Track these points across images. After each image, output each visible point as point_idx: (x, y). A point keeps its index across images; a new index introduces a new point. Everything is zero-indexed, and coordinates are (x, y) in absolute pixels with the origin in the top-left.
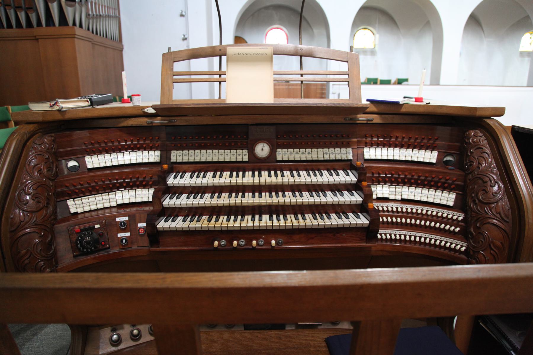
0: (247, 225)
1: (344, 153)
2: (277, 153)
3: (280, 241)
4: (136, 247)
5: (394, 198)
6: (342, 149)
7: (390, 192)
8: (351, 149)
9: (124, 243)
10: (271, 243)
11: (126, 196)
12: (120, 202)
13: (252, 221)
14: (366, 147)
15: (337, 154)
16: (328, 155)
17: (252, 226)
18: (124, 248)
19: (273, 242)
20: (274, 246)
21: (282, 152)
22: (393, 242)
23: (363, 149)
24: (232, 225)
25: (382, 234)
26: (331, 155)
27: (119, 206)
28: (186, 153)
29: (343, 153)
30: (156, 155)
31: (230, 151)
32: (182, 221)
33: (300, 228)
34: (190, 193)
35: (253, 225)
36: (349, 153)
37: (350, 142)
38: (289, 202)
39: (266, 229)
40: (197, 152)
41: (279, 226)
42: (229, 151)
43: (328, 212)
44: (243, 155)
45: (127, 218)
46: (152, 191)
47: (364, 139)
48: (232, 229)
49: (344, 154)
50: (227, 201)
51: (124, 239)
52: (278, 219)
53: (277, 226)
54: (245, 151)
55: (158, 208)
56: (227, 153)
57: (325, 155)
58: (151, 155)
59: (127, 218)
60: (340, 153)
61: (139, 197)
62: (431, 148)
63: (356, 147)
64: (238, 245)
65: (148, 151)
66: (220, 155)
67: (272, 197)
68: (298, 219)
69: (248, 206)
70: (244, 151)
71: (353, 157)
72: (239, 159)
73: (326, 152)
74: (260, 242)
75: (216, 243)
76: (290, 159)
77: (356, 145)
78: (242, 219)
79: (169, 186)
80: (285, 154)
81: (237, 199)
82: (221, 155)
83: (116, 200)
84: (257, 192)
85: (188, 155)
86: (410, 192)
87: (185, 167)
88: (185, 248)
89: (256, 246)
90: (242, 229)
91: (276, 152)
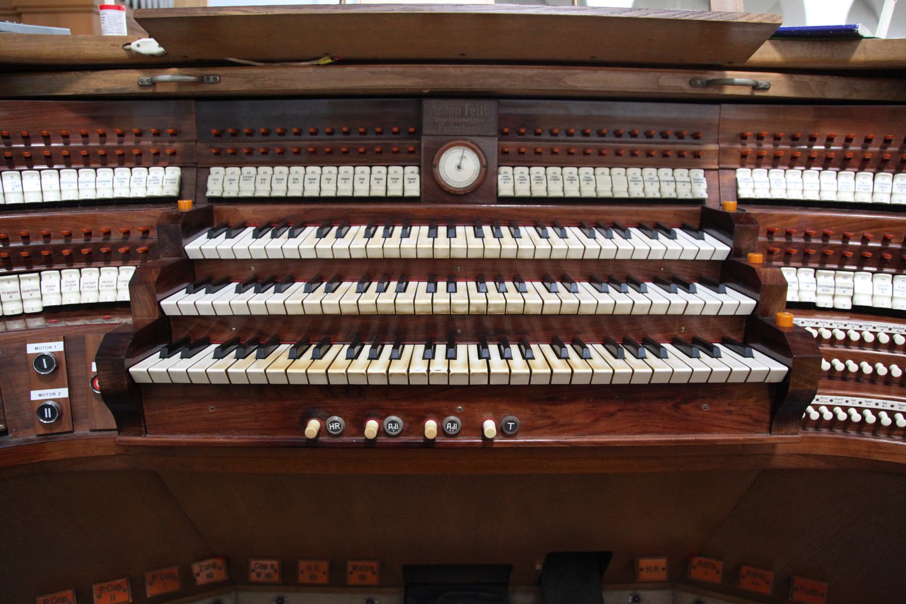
0: (408, 371)
1: (684, 182)
2: (500, 177)
3: (511, 424)
4: (88, 432)
5: (830, 306)
6: (678, 172)
7: (820, 286)
8: (703, 171)
9: (48, 419)
10: (482, 429)
11: (71, 284)
12: (53, 300)
13: (424, 358)
14: (743, 166)
15: (666, 183)
16: (576, 183)
17: (423, 374)
18: (48, 432)
19: (490, 427)
20: (492, 439)
21: (513, 175)
22: (882, 436)
23: (735, 173)
24: (363, 368)
25: (848, 407)
26: (648, 184)
27: (50, 312)
28: (249, 173)
29: (682, 182)
30: (167, 180)
31: (626, 172)
32: (212, 357)
33: (532, 383)
34: (386, 278)
35: (428, 370)
36: (698, 181)
37: (699, 151)
38: (536, 305)
39: (467, 383)
40: (297, 172)
41: (510, 374)
42: (366, 169)
43: (581, 337)
44: (406, 181)
45: (58, 346)
46: (128, 272)
47: (739, 146)
48: (363, 382)
49: (684, 185)
50: (352, 299)
51: (48, 406)
52: (506, 356)
53: (505, 374)
54: (412, 171)
55: (145, 315)
56: (362, 176)
57: (632, 185)
58: (156, 179)
59: (58, 346)
60: (672, 181)
61: (109, 288)
62: (158, 159)
63: (717, 167)
64: (381, 432)
65: (131, 168)
66: (342, 179)
67: (487, 292)
68: (566, 356)
69: (415, 316)
70: (408, 169)
71: (708, 192)
72: (395, 190)
73: (633, 178)
74: (449, 426)
75: (313, 426)
76: (535, 194)
77: (716, 161)
78: (396, 355)
79: (191, 257)
80: (522, 179)
81: (382, 294)
82: (345, 179)
83: (852, 294)
84: (442, 280)
85: (253, 179)
86: (879, 289)
87: (246, 211)
88: (220, 439)
89: (437, 436)
90: (393, 382)
91: (497, 173)
